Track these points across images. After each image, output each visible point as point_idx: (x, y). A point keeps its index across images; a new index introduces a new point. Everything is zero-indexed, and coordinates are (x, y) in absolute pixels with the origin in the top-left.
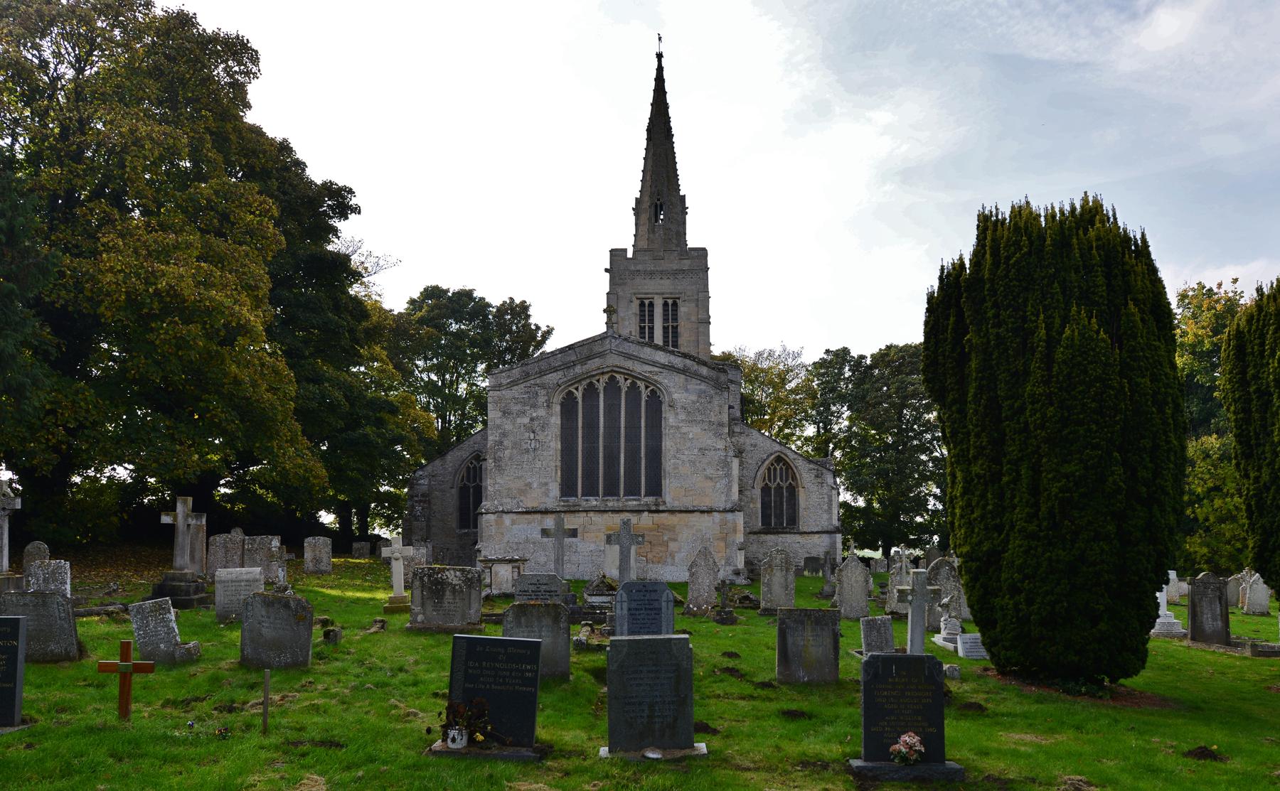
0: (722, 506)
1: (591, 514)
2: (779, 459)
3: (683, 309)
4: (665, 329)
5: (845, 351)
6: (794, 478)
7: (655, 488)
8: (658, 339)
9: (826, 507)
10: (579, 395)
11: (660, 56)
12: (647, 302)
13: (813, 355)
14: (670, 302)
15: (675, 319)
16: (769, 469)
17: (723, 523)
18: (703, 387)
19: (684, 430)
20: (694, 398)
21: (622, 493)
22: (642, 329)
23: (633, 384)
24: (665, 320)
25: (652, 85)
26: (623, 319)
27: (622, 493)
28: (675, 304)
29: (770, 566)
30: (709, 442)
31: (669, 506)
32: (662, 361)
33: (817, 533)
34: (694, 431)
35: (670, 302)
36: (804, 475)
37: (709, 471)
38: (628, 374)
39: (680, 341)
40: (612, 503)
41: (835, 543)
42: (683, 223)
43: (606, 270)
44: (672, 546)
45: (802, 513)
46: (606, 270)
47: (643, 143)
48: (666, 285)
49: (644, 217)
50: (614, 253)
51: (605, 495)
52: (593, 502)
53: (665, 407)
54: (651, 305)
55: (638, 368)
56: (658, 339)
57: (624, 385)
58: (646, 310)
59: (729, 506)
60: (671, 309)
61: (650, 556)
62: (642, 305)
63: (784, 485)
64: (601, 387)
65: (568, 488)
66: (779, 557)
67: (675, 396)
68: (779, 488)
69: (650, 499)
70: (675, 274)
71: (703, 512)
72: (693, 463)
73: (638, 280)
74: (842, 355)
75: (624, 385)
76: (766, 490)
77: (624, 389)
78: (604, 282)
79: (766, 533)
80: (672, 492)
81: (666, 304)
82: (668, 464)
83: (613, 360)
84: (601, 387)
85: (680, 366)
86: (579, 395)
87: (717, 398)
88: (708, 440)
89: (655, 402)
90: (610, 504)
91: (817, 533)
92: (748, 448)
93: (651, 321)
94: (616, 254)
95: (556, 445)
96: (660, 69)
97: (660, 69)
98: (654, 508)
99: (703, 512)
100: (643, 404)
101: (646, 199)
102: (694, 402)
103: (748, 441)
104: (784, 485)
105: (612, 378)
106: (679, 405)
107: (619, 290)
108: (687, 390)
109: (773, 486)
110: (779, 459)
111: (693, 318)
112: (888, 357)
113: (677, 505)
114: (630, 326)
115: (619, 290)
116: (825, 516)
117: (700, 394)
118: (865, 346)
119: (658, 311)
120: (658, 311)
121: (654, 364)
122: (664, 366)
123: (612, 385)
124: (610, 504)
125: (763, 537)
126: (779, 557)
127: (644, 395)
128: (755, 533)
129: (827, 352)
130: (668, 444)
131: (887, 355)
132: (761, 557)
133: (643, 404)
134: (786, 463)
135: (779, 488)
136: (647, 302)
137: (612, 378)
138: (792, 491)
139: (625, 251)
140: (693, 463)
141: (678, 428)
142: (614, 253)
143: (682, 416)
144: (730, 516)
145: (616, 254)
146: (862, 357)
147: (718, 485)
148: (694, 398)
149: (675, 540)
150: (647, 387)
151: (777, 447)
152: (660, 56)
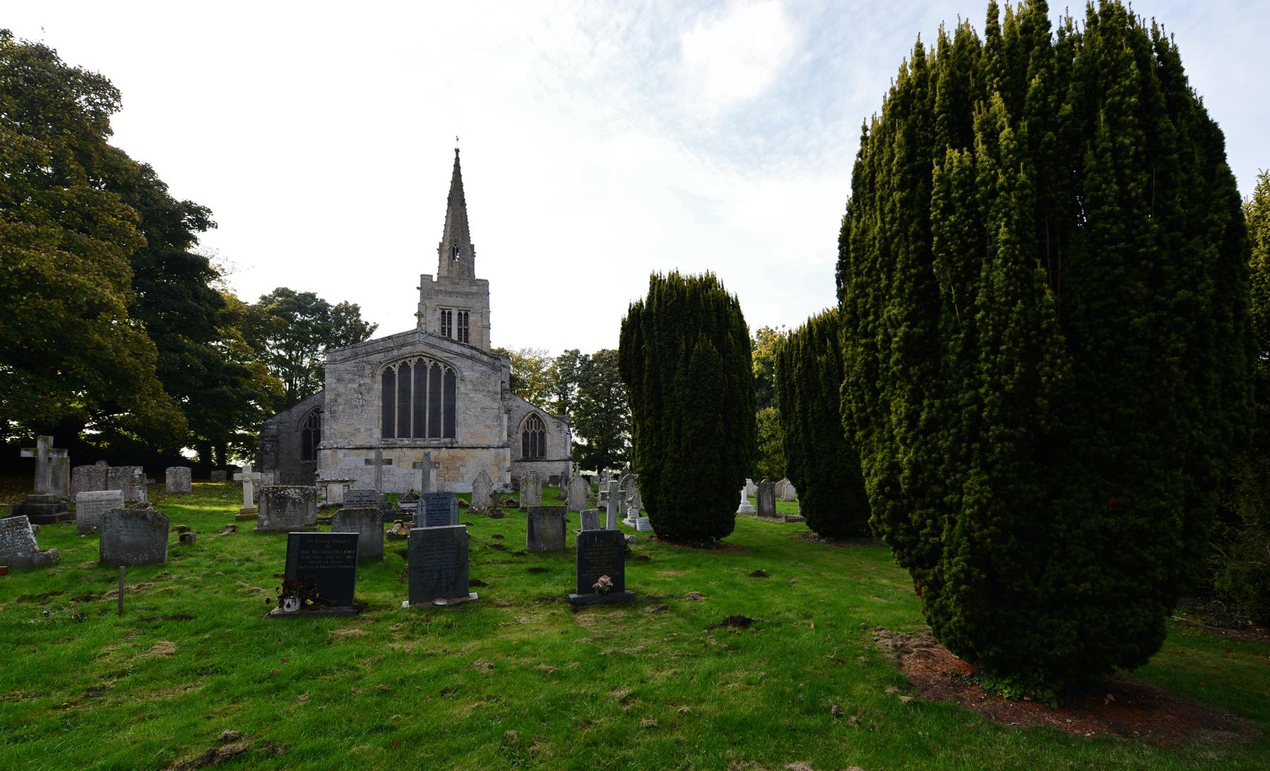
2: (534, 416)
3: (472, 318)
4: (460, 330)
7: (451, 433)
10: (396, 370)
11: (457, 151)
13: (556, 353)
15: (466, 324)
17: (497, 455)
22: (443, 329)
23: (436, 364)
24: (460, 324)
28: (466, 314)
34: (478, 397)
37: (488, 422)
38: (432, 358)
40: (420, 442)
44: (462, 469)
48: (460, 302)
49: (445, 256)
50: (423, 277)
52: (406, 441)
54: (450, 313)
55: (439, 354)
57: (429, 365)
58: (446, 316)
62: (443, 313)
64: (412, 365)
65: (387, 432)
69: (447, 440)
70: (467, 295)
73: (440, 297)
74: (575, 354)
75: (429, 365)
76: (525, 435)
77: (443, 373)
80: (462, 436)
81: (460, 314)
82: (460, 417)
83: (421, 348)
84: (412, 365)
86: (396, 370)
88: (488, 402)
93: (450, 324)
94: (425, 278)
95: (378, 403)
96: (457, 159)
97: (457, 159)
105: (421, 360)
107: (427, 303)
110: (534, 416)
113: (466, 443)
115: (427, 303)
119: (455, 318)
120: (455, 318)
121: (451, 352)
122: (457, 354)
123: (420, 365)
125: (524, 464)
130: (459, 404)
137: (421, 360)
138: (542, 435)
142: (423, 277)
143: (470, 387)
144: (501, 450)
145: (425, 278)
148: (478, 375)
152: (457, 151)
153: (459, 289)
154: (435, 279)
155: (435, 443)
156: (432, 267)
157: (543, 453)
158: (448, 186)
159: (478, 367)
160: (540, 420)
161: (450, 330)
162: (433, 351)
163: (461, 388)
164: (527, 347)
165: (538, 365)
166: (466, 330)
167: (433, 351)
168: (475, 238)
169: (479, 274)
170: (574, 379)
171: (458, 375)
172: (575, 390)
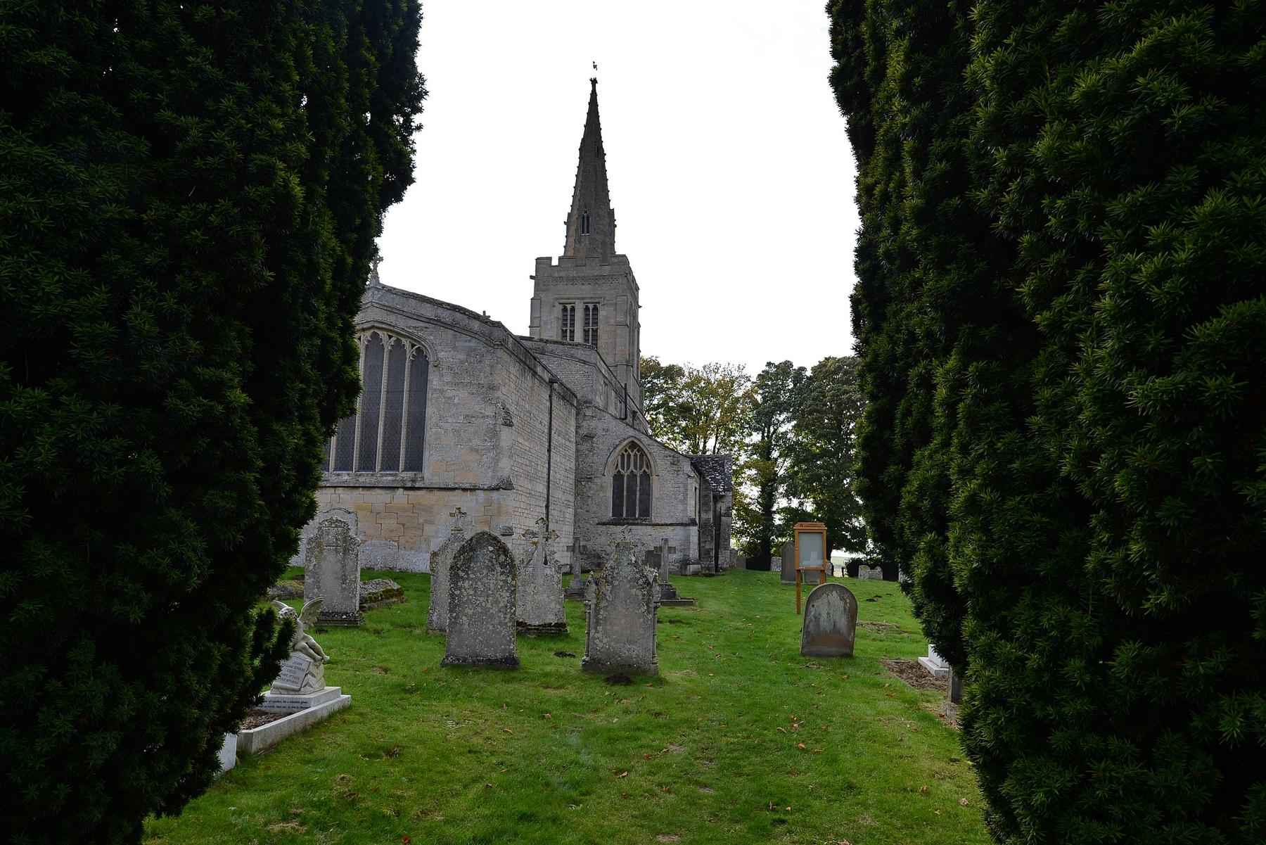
0: (487, 483)
1: (340, 491)
2: (633, 445)
3: (602, 313)
4: (586, 332)
5: (787, 364)
6: (648, 466)
7: (415, 464)
8: (579, 337)
9: (681, 497)
11: (594, 82)
12: (569, 307)
13: (755, 370)
14: (591, 306)
15: (595, 323)
16: (623, 456)
17: (489, 504)
18: (473, 344)
19: (449, 394)
20: (462, 357)
21: (378, 467)
22: (564, 332)
23: (398, 341)
25: (586, 108)
26: (546, 323)
27: (378, 467)
28: (595, 309)
29: (319, 545)
30: (477, 408)
31: (427, 483)
32: (428, 315)
33: (671, 525)
34: (460, 395)
35: (591, 306)
36: (659, 462)
37: (476, 442)
38: (391, 332)
39: (600, 343)
40: (365, 478)
41: (689, 536)
42: (612, 234)
43: (532, 277)
44: (429, 529)
45: (655, 503)
46: (532, 277)
47: (576, 162)
48: (587, 290)
49: (573, 228)
50: (540, 261)
51: (360, 469)
52: (345, 477)
53: (431, 368)
54: (573, 309)
56: (579, 337)
57: (388, 343)
58: (567, 313)
59: (494, 483)
60: (592, 313)
61: (402, 540)
62: (565, 309)
63: (638, 473)
66: (333, 531)
67: (441, 355)
68: (633, 476)
69: (410, 474)
70: (596, 279)
71: (465, 490)
72: (457, 432)
73: (561, 286)
74: (785, 368)
75: (388, 343)
76: (618, 478)
77: (387, 348)
78: (529, 289)
79: (616, 524)
80: (431, 472)
81: (587, 309)
85: (449, 320)
87: (489, 357)
89: (421, 363)
90: (361, 479)
91: (671, 525)
92: (600, 433)
93: (572, 325)
94: (542, 263)
96: (594, 95)
97: (594, 95)
98: (409, 485)
99: (465, 490)
100: (408, 364)
101: (575, 212)
102: (462, 362)
103: (600, 425)
104: (638, 473)
105: (375, 335)
106: (445, 366)
107: (543, 296)
108: (455, 348)
109: (626, 473)
110: (633, 445)
111: (612, 322)
112: (827, 369)
113: (436, 481)
114: (552, 332)
115: (543, 296)
116: (680, 507)
117: (470, 352)
118: (807, 360)
119: (579, 315)
120: (579, 315)
121: (418, 318)
122: (429, 321)
124: (361, 479)
125: (613, 529)
126: (333, 531)
127: (409, 353)
128: (604, 524)
129: (769, 364)
131: (825, 365)
132: (609, 549)
133: (408, 364)
134: (640, 450)
135: (633, 476)
136: (569, 307)
137: (375, 335)
138: (646, 477)
139: (550, 259)
140: (457, 432)
141: (442, 391)
142: (540, 261)
143: (448, 379)
144: (495, 495)
145: (542, 263)
146: (802, 369)
147: (485, 459)
148: (462, 357)
149: (432, 523)
150: (413, 346)
151: (631, 432)
152: (594, 82)
153: (587, 272)
154: (555, 262)
155: (388, 479)
156: (554, 246)
157: (646, 511)
158: (580, 133)
159: (465, 342)
160: (643, 454)
161: (572, 332)
162: (391, 319)
163: (434, 381)
164: (711, 360)
165: (728, 385)
166: (595, 331)
167: (391, 319)
168: (617, 199)
169: (619, 249)
170: (782, 408)
171: (431, 358)
172: (786, 426)
